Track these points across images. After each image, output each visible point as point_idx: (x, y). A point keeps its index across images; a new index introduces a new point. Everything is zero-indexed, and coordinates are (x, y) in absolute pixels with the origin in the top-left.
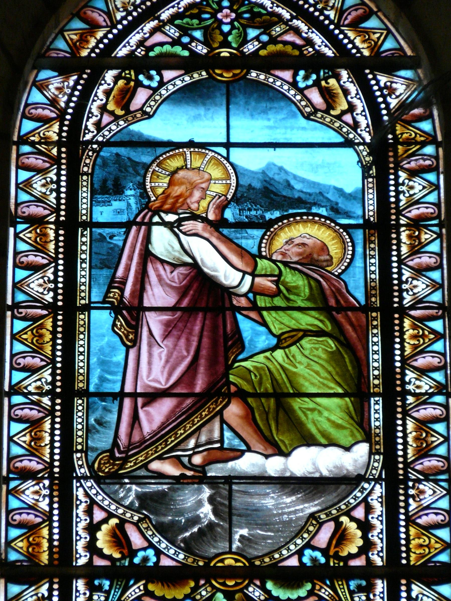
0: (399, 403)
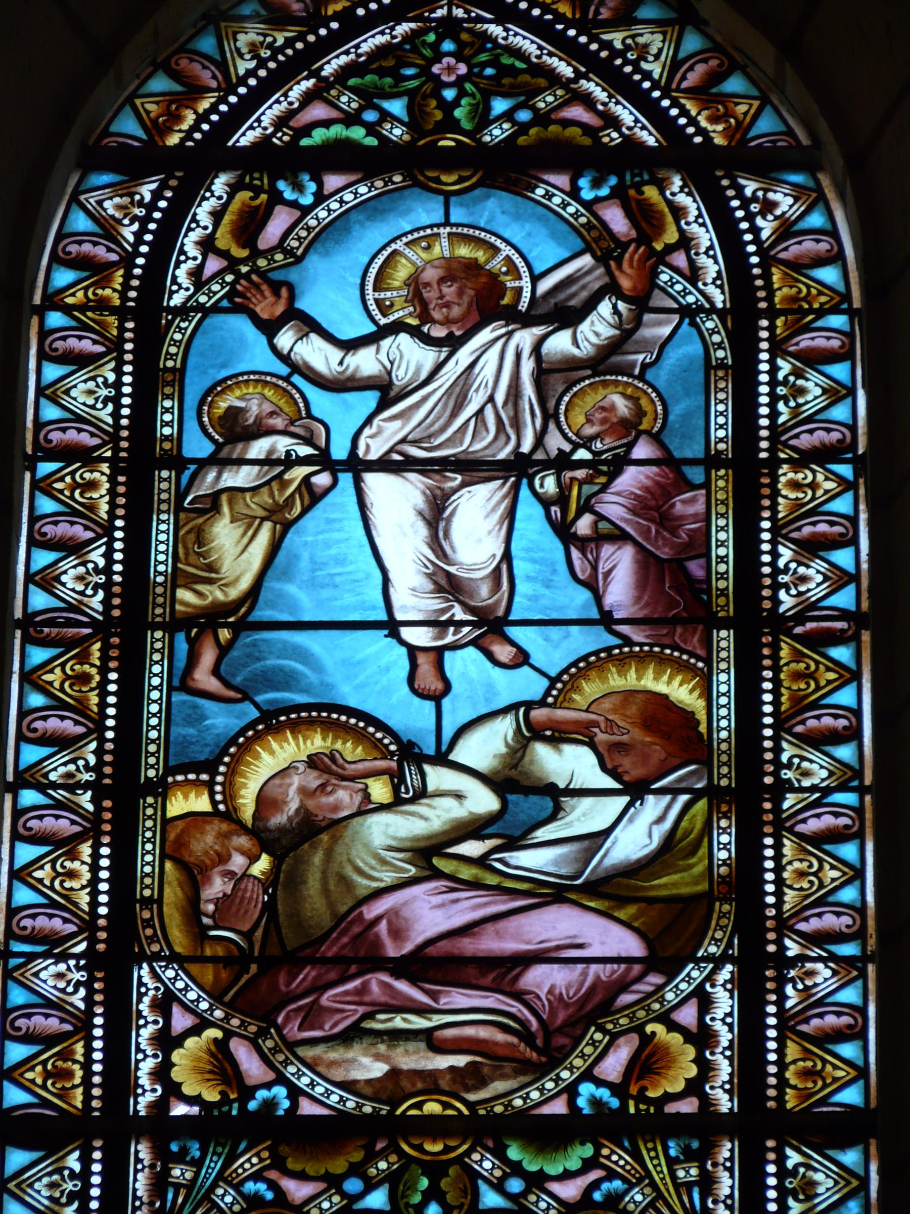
0: (767, 806)
